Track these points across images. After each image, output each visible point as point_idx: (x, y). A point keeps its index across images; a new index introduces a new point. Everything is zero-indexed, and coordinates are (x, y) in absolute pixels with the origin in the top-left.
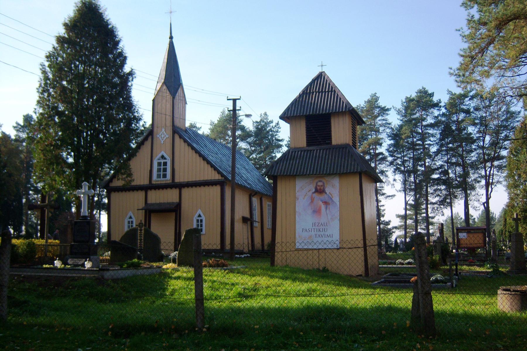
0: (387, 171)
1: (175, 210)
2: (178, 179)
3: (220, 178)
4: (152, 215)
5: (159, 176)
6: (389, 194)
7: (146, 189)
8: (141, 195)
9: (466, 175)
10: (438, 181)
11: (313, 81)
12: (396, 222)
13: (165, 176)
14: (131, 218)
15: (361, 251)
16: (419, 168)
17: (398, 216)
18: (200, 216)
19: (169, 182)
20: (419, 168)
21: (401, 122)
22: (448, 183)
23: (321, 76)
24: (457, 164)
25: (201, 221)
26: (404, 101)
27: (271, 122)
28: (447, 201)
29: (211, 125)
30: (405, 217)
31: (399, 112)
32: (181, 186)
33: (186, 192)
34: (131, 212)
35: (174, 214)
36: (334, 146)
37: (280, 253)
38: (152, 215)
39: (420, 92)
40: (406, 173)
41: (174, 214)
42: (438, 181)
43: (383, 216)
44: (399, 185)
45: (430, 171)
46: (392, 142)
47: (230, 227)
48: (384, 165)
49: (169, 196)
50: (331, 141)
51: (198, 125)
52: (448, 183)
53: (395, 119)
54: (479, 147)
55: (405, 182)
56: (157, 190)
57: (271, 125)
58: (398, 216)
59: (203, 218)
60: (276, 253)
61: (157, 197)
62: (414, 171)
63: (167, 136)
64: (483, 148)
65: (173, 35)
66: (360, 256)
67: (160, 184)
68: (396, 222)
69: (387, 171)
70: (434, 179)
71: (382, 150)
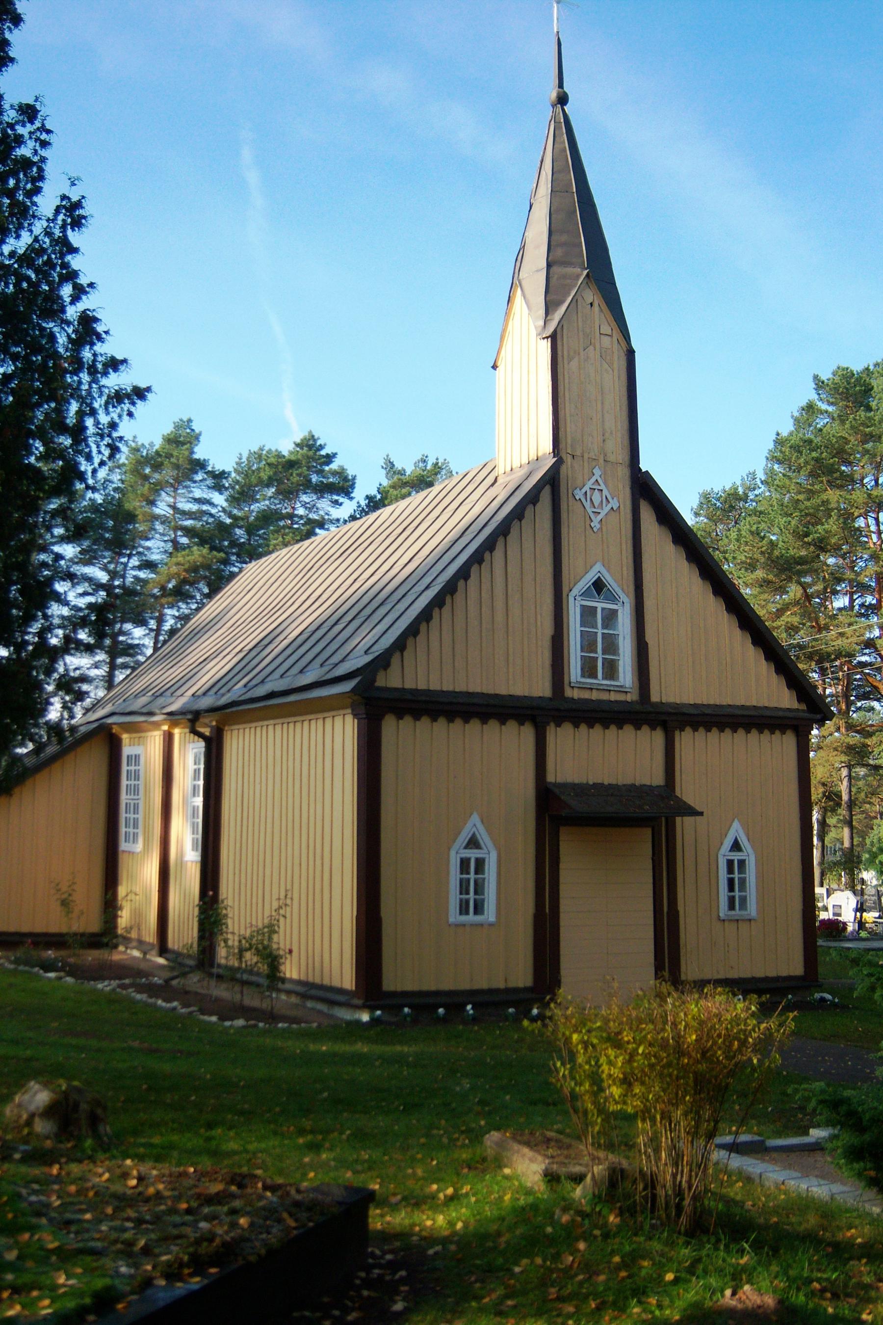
1: (651, 818)
2: (672, 688)
3: (795, 705)
4: (563, 830)
5: (589, 669)
7: (542, 714)
8: (517, 740)
13: (611, 670)
14: (473, 843)
18: (473, 843)
19: (629, 698)
25: (480, 864)
32: (671, 720)
33: (689, 743)
34: (475, 818)
35: (647, 833)
38: (563, 830)
41: (647, 833)
47: (495, 898)
49: (626, 759)
56: (458, 723)
59: (749, 854)
61: (588, 758)
63: (614, 504)
65: (566, 88)
67: (600, 702)
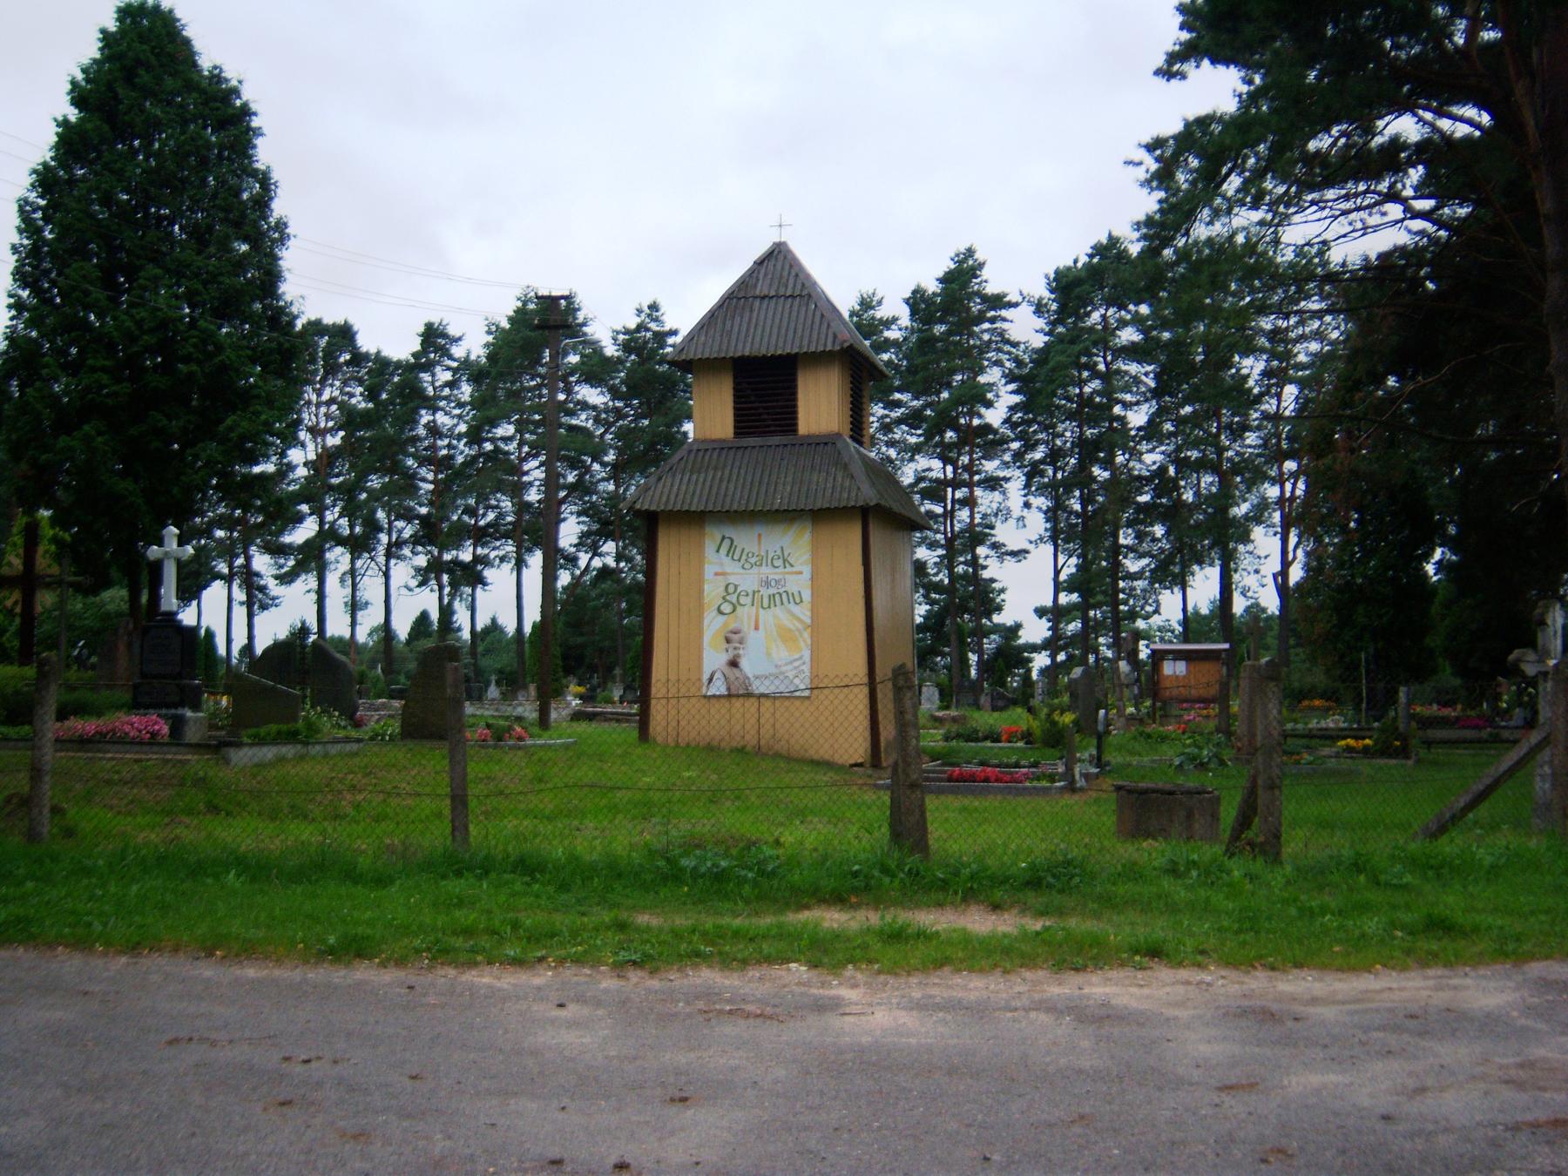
0: (1007, 480)
6: (1013, 546)
9: (1224, 499)
10: (1148, 513)
11: (760, 263)
12: (1035, 631)
15: (862, 694)
16: (1096, 471)
17: (1041, 612)
20: (1096, 471)
21: (1047, 338)
22: (1173, 514)
23: (777, 260)
24: (1202, 466)
26: (1052, 276)
27: (674, 333)
28: (1171, 572)
29: (489, 332)
30: (1055, 614)
31: (1039, 308)
36: (804, 437)
37: (664, 702)
39: (1099, 250)
40: (1057, 492)
42: (1148, 513)
43: (999, 609)
44: (1037, 523)
45: (1124, 486)
46: (1017, 399)
48: (997, 462)
50: (796, 425)
51: (453, 331)
52: (1173, 514)
53: (1026, 329)
54: (1266, 416)
55: (1051, 515)
57: (671, 340)
58: (1041, 612)
60: (653, 702)
62: (1081, 478)
64: (1276, 418)
66: (861, 707)
68: (1035, 631)
69: (1007, 480)
70: (1138, 504)
71: (994, 416)
